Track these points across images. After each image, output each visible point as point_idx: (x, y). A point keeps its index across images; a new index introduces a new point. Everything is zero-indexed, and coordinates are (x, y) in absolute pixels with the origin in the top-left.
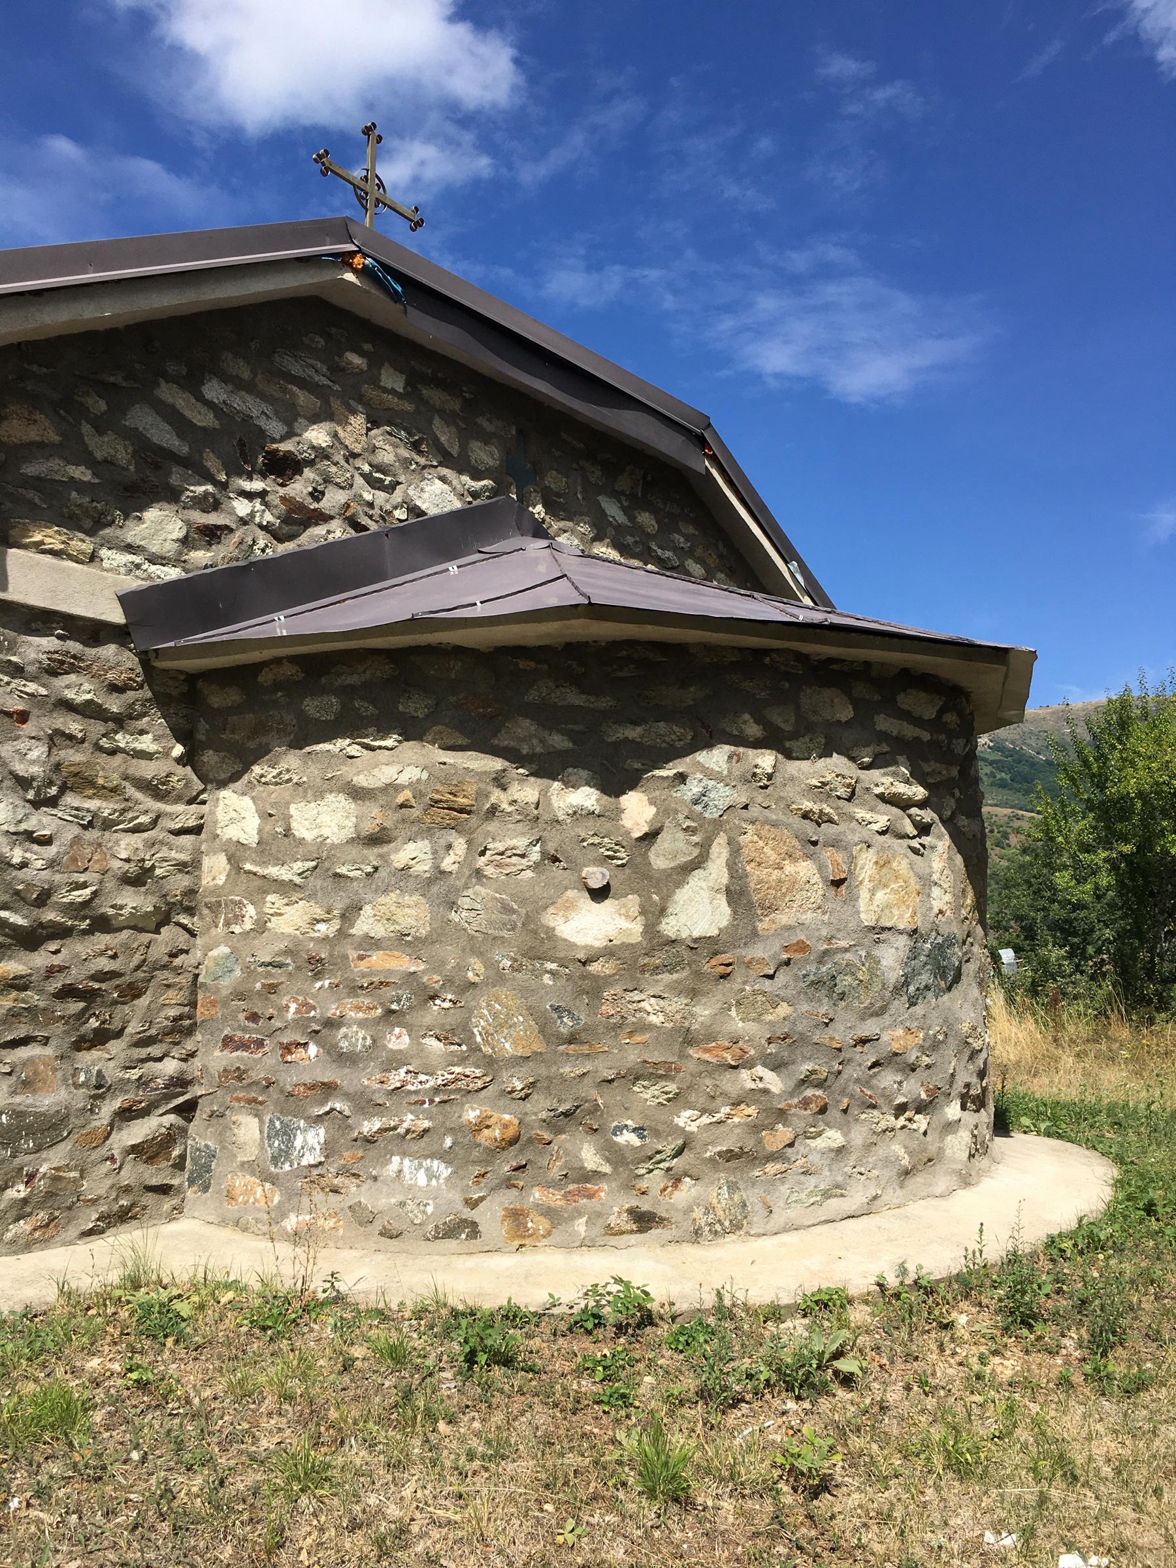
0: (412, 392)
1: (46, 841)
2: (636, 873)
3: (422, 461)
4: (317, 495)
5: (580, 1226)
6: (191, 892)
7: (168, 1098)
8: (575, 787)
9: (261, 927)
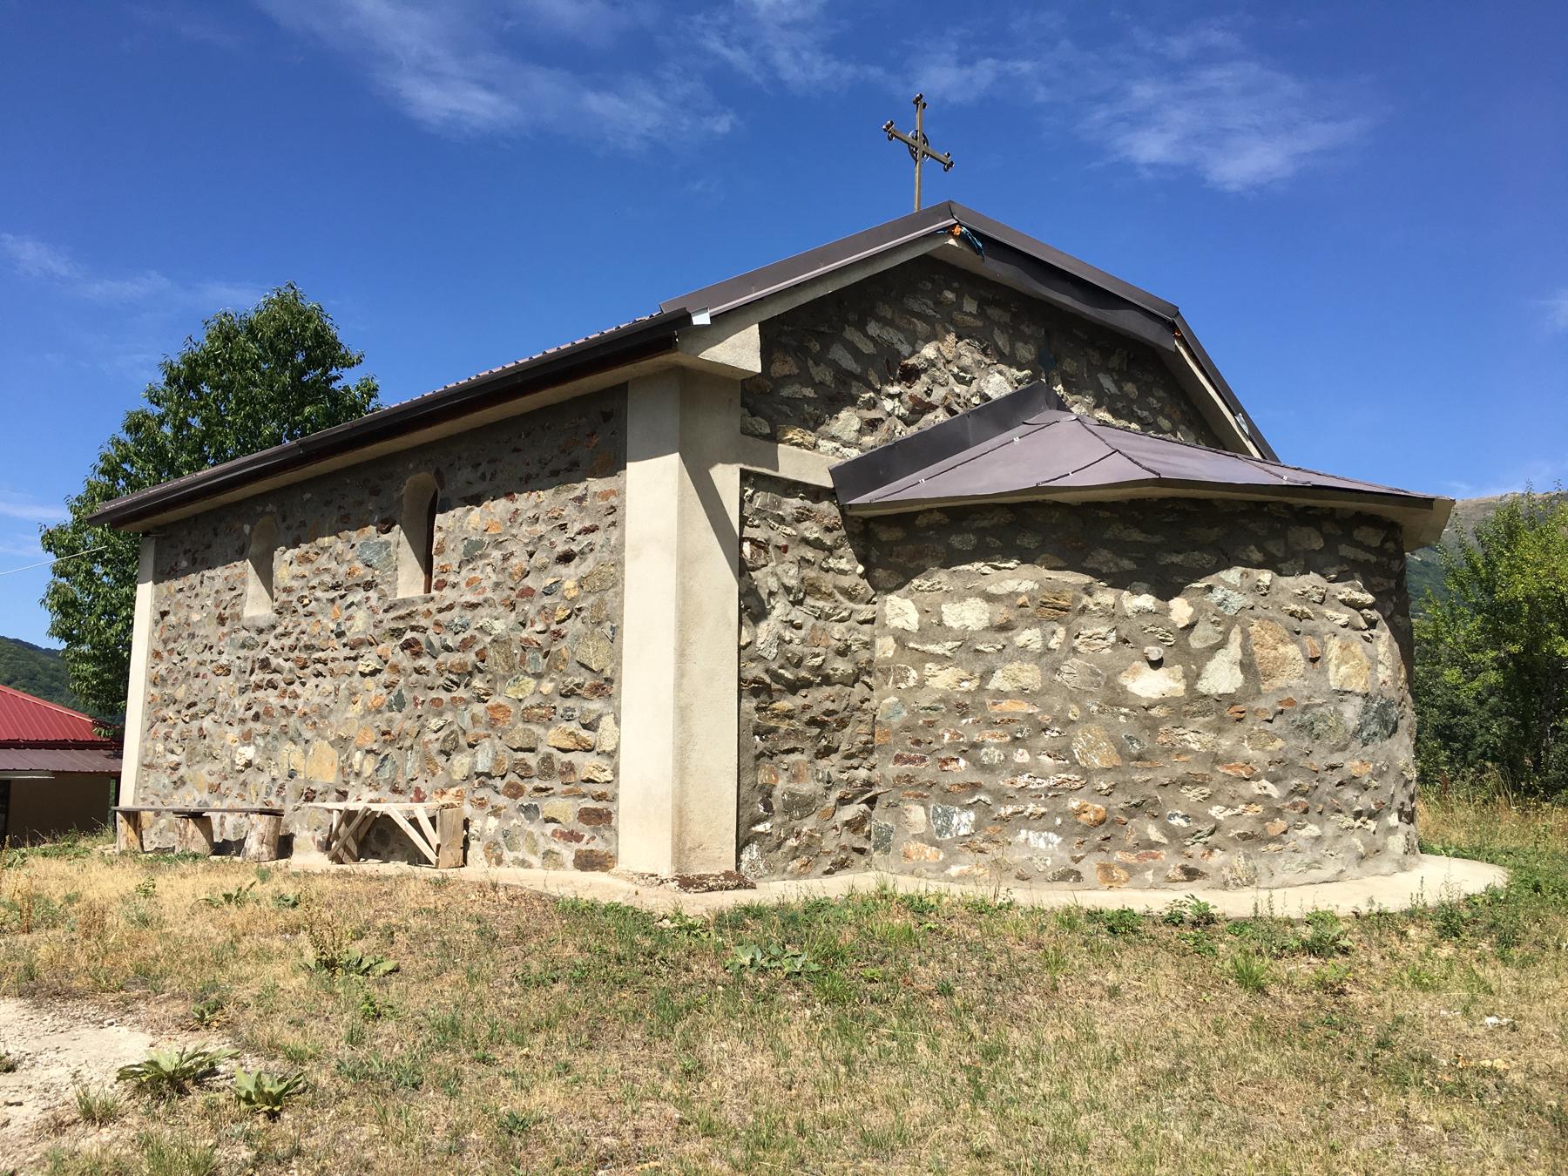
0: (981, 314)
1: (799, 627)
2: (1182, 651)
3: (988, 361)
4: (929, 393)
5: (1149, 875)
6: (870, 662)
7: (863, 793)
8: (1139, 594)
9: (921, 684)
